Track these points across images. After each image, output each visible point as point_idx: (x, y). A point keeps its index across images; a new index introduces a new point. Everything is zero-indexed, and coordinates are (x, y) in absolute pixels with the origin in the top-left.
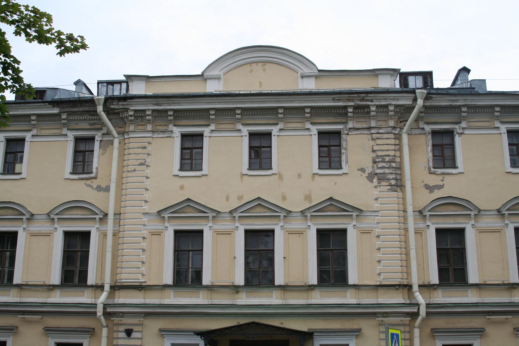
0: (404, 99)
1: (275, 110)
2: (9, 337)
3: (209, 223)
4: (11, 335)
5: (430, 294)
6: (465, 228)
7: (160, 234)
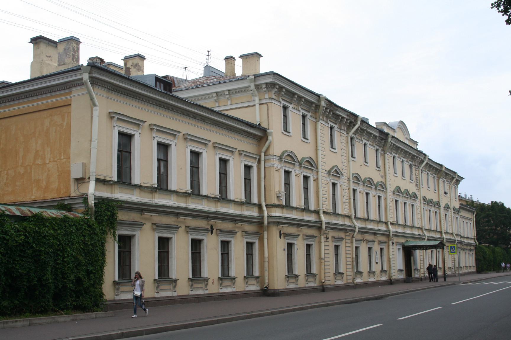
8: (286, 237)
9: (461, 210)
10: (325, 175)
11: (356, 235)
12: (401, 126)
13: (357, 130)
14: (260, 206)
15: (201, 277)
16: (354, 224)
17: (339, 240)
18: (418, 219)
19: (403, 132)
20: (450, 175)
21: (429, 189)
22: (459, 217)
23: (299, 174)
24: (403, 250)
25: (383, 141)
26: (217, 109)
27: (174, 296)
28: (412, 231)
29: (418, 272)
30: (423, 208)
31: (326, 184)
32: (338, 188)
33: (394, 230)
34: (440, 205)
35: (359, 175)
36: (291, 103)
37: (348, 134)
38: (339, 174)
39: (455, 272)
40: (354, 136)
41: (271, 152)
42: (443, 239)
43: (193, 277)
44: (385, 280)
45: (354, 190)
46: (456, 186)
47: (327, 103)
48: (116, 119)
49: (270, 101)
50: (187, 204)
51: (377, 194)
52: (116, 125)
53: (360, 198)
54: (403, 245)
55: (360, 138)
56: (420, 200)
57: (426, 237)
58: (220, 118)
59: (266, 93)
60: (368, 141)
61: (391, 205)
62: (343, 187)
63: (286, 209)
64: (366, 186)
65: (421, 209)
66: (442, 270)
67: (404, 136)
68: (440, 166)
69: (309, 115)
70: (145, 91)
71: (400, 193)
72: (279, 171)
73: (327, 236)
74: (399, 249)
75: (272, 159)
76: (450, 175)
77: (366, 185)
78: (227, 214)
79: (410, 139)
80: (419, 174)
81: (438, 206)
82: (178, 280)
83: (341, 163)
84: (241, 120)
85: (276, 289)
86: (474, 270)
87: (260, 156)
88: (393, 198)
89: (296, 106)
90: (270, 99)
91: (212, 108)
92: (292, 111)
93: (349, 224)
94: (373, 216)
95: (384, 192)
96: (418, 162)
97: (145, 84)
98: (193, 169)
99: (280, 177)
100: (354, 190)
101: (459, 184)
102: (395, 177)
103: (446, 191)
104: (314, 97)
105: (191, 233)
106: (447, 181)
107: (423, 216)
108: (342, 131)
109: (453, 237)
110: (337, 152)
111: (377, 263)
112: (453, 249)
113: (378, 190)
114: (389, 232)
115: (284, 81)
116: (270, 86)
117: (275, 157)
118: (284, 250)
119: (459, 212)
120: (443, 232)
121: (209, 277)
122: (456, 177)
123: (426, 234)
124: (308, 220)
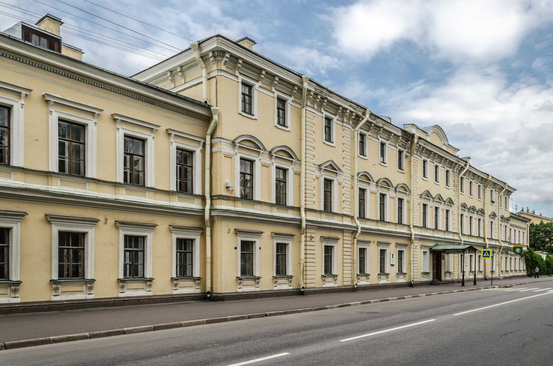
0: (211, 43)
1: (260, 70)
2: (91, 228)
3: (21, 100)
4: (93, 227)
5: (235, 204)
6: (12, 106)
7: (268, 167)
8: (238, 234)
9: (511, 219)
10: (488, 218)
11: (359, 235)
12: (437, 131)
13: (466, 172)
14: (203, 198)
15: (84, 279)
16: (501, 244)
17: (329, 240)
18: (454, 224)
19: (439, 137)
20: (499, 186)
21: (506, 209)
22: (509, 225)
23: (232, 155)
24: (431, 253)
25: (409, 142)
26: (174, 91)
27: (257, 291)
28: (496, 243)
29: (450, 275)
30: (501, 225)
31: (315, 179)
32: (428, 208)
33: (489, 243)
34: (484, 212)
35: (467, 205)
36: (335, 115)
37: (354, 128)
38: (336, 170)
39: (499, 275)
40: (463, 176)
41: (218, 134)
42: (486, 244)
43: (60, 278)
44: (404, 283)
45: (462, 215)
46: (508, 197)
47: (315, 87)
48: (173, 136)
49: (219, 74)
50: (49, 187)
51: (397, 196)
52: (174, 141)
53: (466, 221)
54: (430, 249)
55: (375, 136)
56: (498, 218)
57: (463, 241)
58: (18, 47)
59: (214, 64)
60: (473, 180)
61: (488, 225)
62: (454, 213)
63: (381, 224)
64: (424, 198)
65: (498, 225)
66: (483, 273)
67: (442, 142)
68: (487, 176)
69: (335, 118)
70: (62, 62)
71: (441, 200)
72: (231, 158)
73: (311, 236)
74: (425, 253)
75: (219, 143)
76: (499, 186)
77: (380, 185)
78: (124, 201)
79: (449, 144)
80: (458, 181)
81: (482, 213)
82: (261, 278)
83: (342, 159)
84: (165, 91)
85: (219, 293)
86: (525, 273)
87: (205, 139)
88: (489, 220)
89: (268, 86)
90: (219, 71)
91: (170, 90)
92: (258, 90)
93: (350, 224)
94: (475, 233)
95: (407, 194)
96: (498, 188)
97: (138, 81)
98: (70, 143)
99: (443, 213)
100: (462, 215)
101: (510, 195)
102: (480, 202)
103: (494, 200)
104: (295, 78)
105: (239, 236)
106: (495, 191)
107: (500, 230)
108: (344, 124)
109: (499, 243)
110: (387, 166)
111: (392, 265)
112: (486, 254)
113: (398, 192)
114: (411, 235)
115: (294, 76)
116: (218, 54)
117: (222, 140)
118: (236, 248)
119: (508, 221)
120: (486, 238)
121: (338, 275)
122: (506, 187)
123: (488, 242)
124: (281, 216)
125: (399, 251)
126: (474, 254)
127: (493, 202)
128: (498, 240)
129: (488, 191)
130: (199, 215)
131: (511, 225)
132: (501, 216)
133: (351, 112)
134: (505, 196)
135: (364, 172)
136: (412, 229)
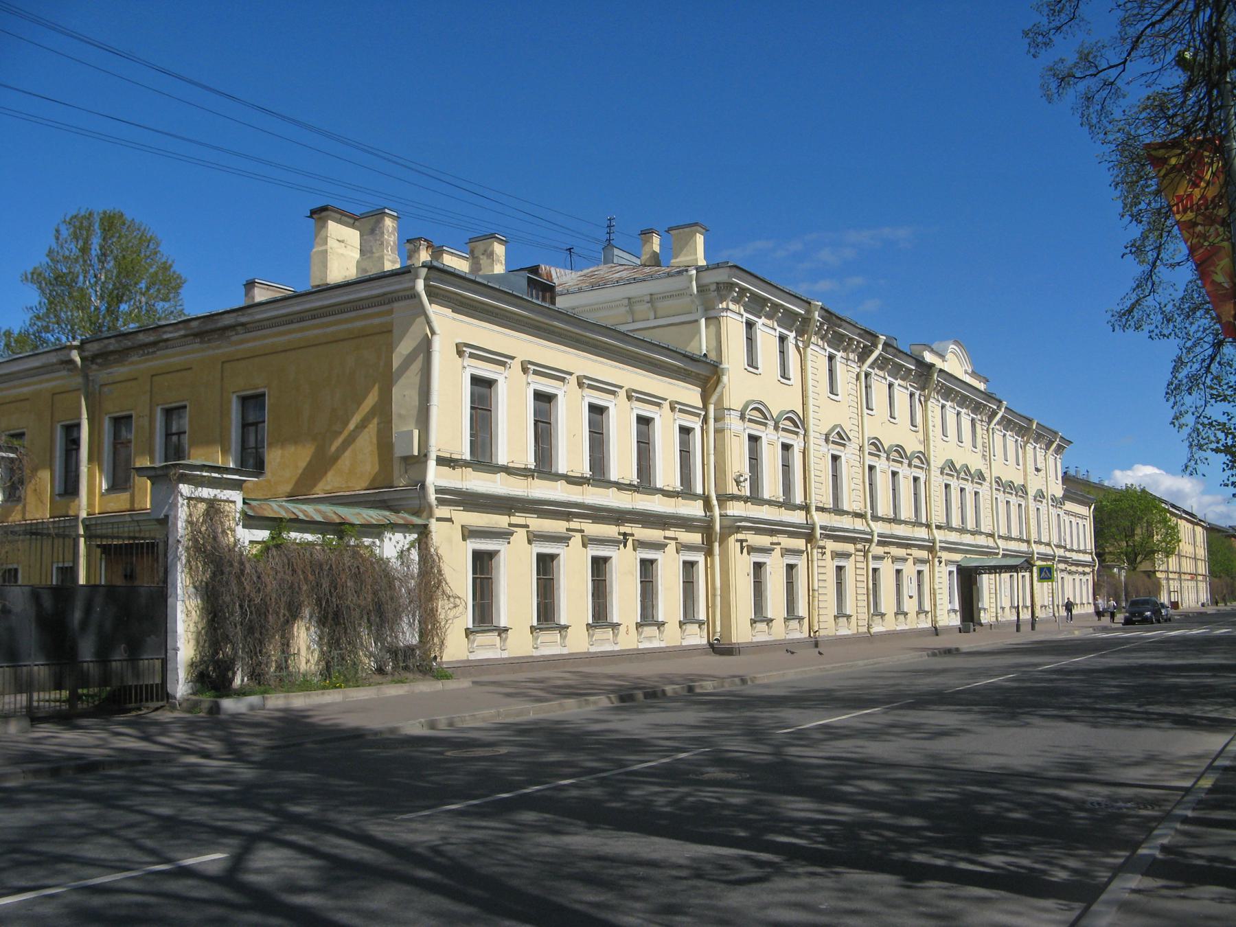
21: (1018, 467)
45: (871, 468)
53: (883, 482)
94: (1055, 541)
100: (871, 468)
125: (837, 567)
126: (1015, 574)
127: (1038, 470)
128: (992, 535)
129: (1029, 447)
130: (706, 527)
131: (1068, 513)
132: (869, 439)
133: (859, 342)
134: (908, 389)
135: (788, 412)
136: (1033, 545)
